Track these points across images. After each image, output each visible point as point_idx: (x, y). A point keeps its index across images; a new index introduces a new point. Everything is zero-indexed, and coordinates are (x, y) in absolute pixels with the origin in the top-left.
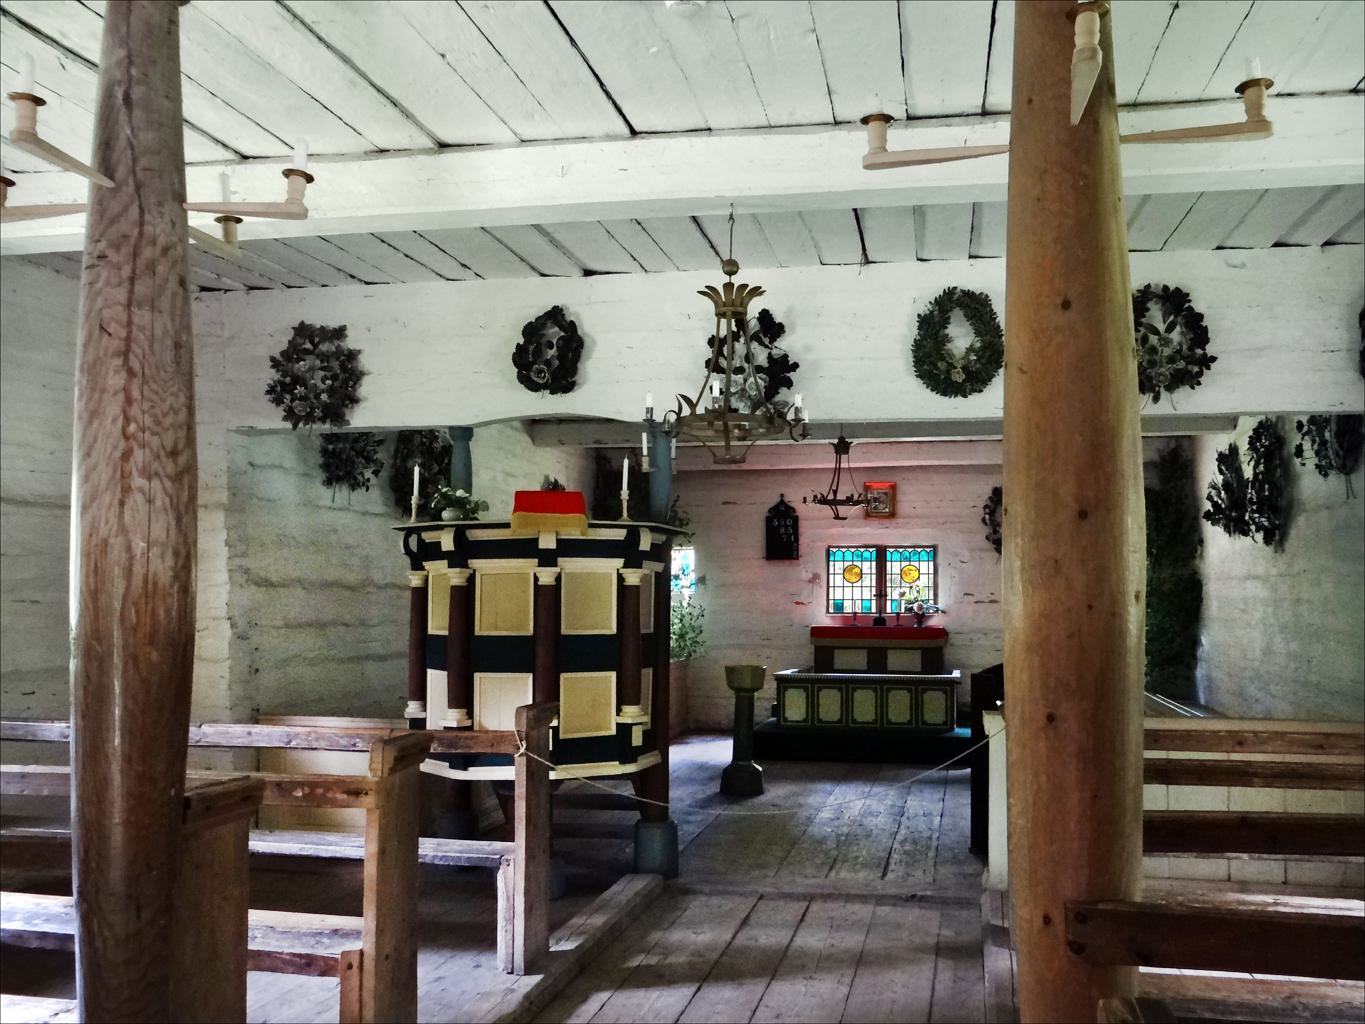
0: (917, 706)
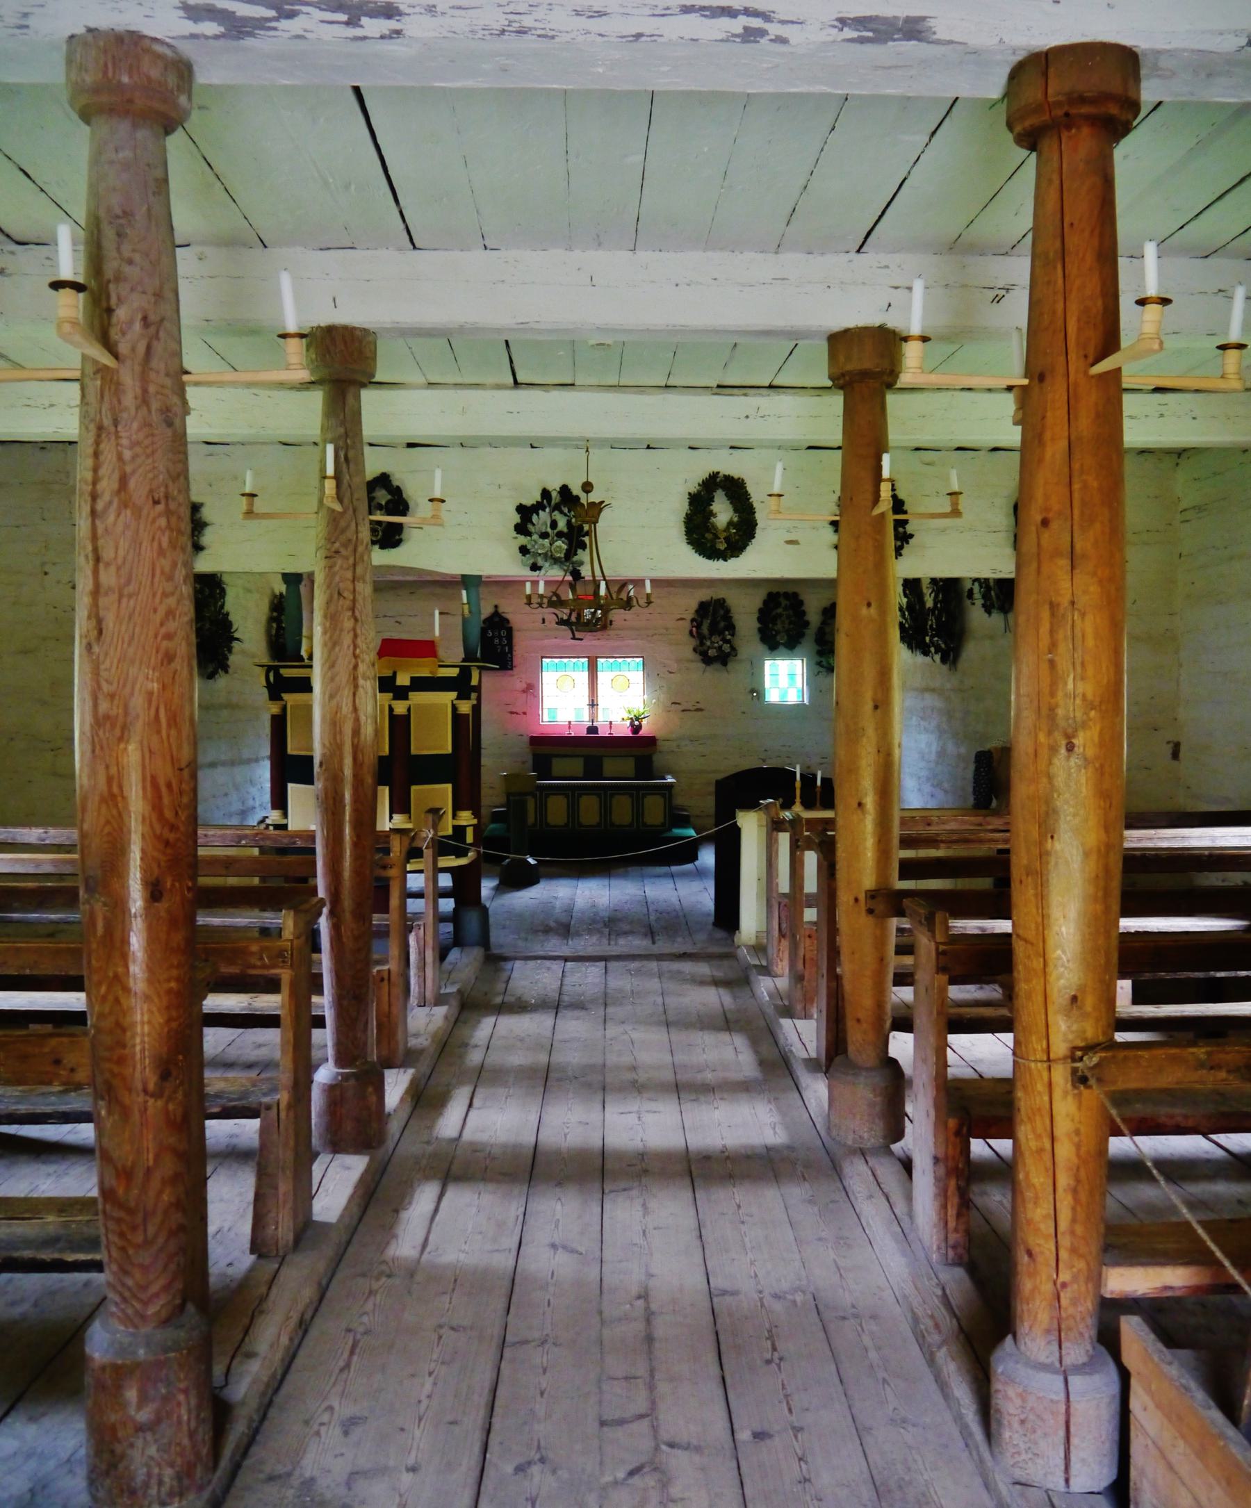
0: (638, 810)
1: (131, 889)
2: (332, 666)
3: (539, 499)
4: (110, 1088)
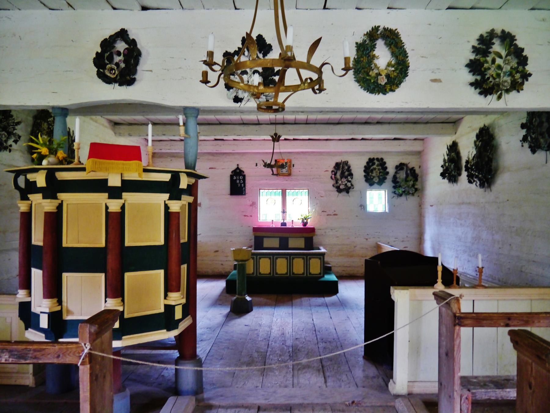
0: (307, 266)
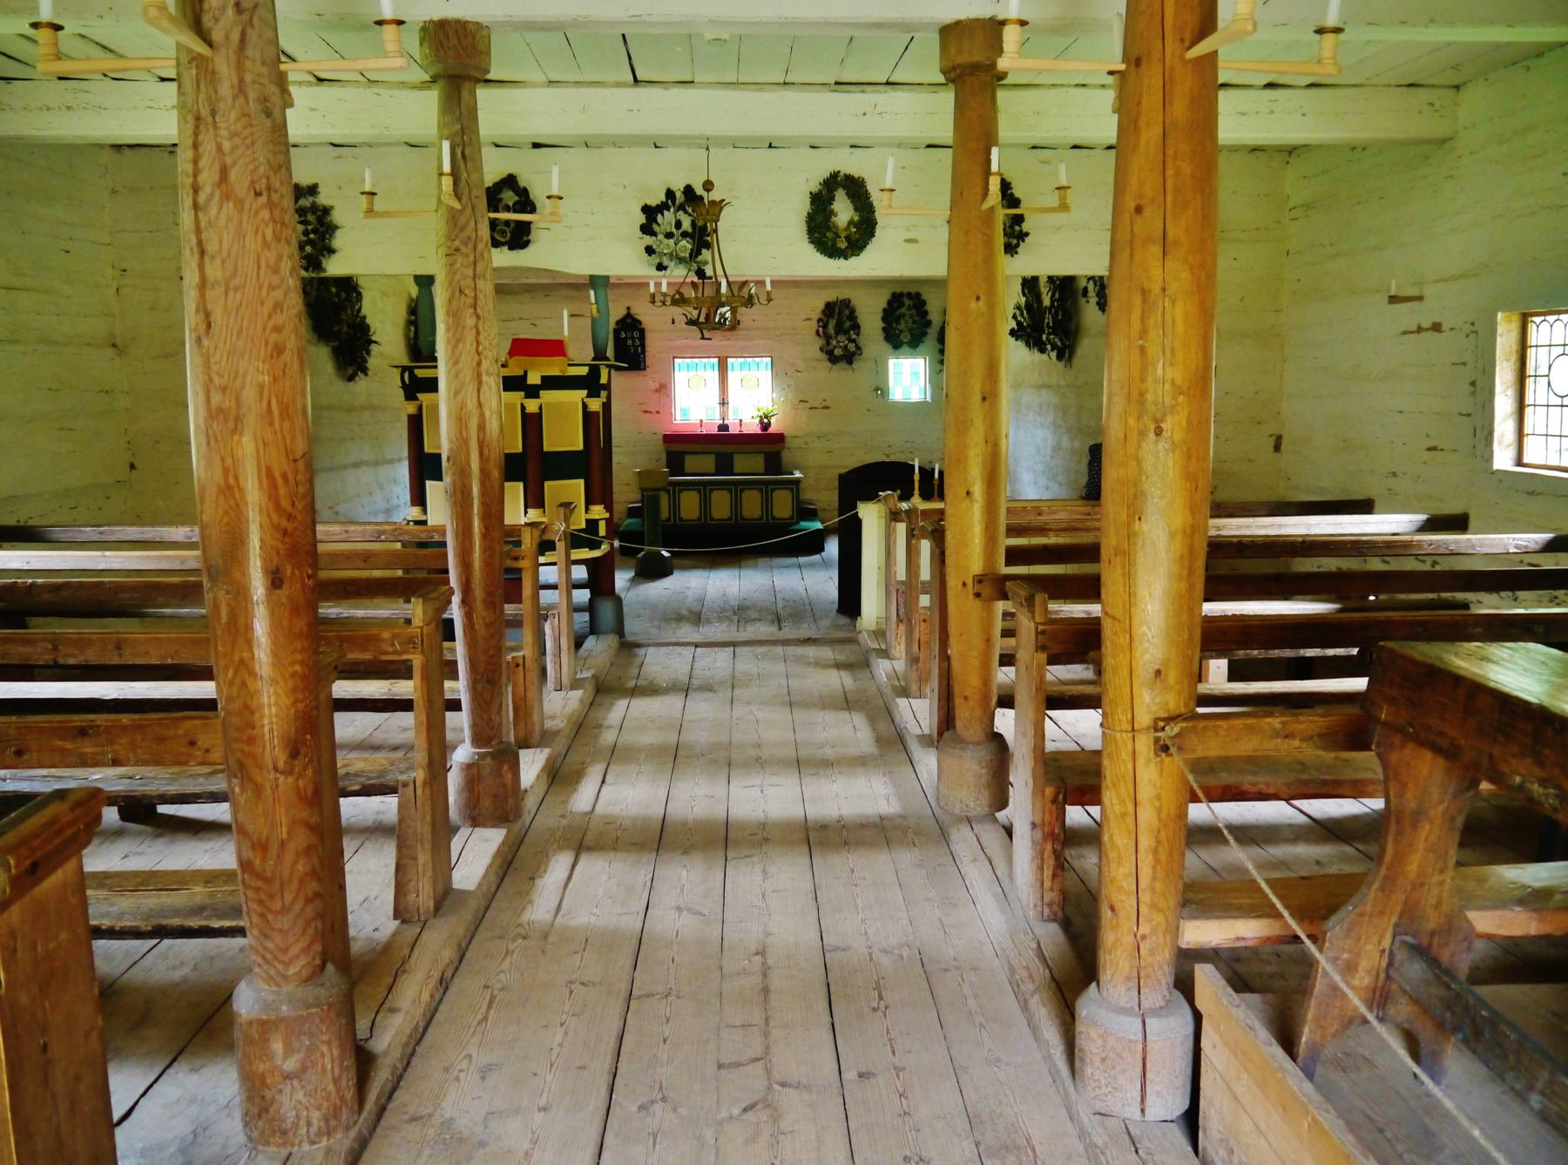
0: (767, 504)
1: (253, 577)
2: (456, 363)
3: (664, 199)
4: (241, 765)
